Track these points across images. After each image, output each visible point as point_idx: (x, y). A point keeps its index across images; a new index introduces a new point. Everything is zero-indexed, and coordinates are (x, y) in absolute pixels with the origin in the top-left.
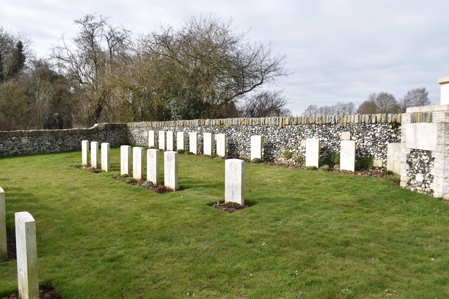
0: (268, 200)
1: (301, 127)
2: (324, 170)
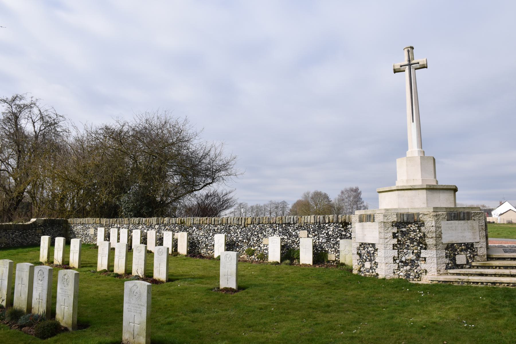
0: (256, 285)
1: (263, 226)
2: (287, 264)
